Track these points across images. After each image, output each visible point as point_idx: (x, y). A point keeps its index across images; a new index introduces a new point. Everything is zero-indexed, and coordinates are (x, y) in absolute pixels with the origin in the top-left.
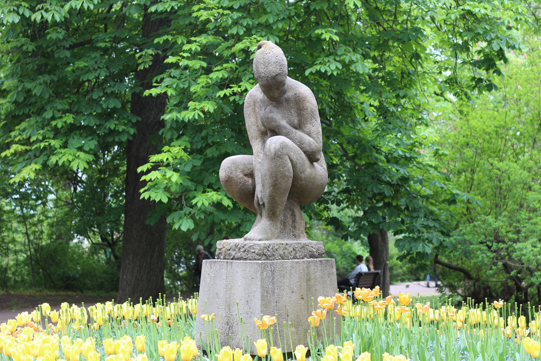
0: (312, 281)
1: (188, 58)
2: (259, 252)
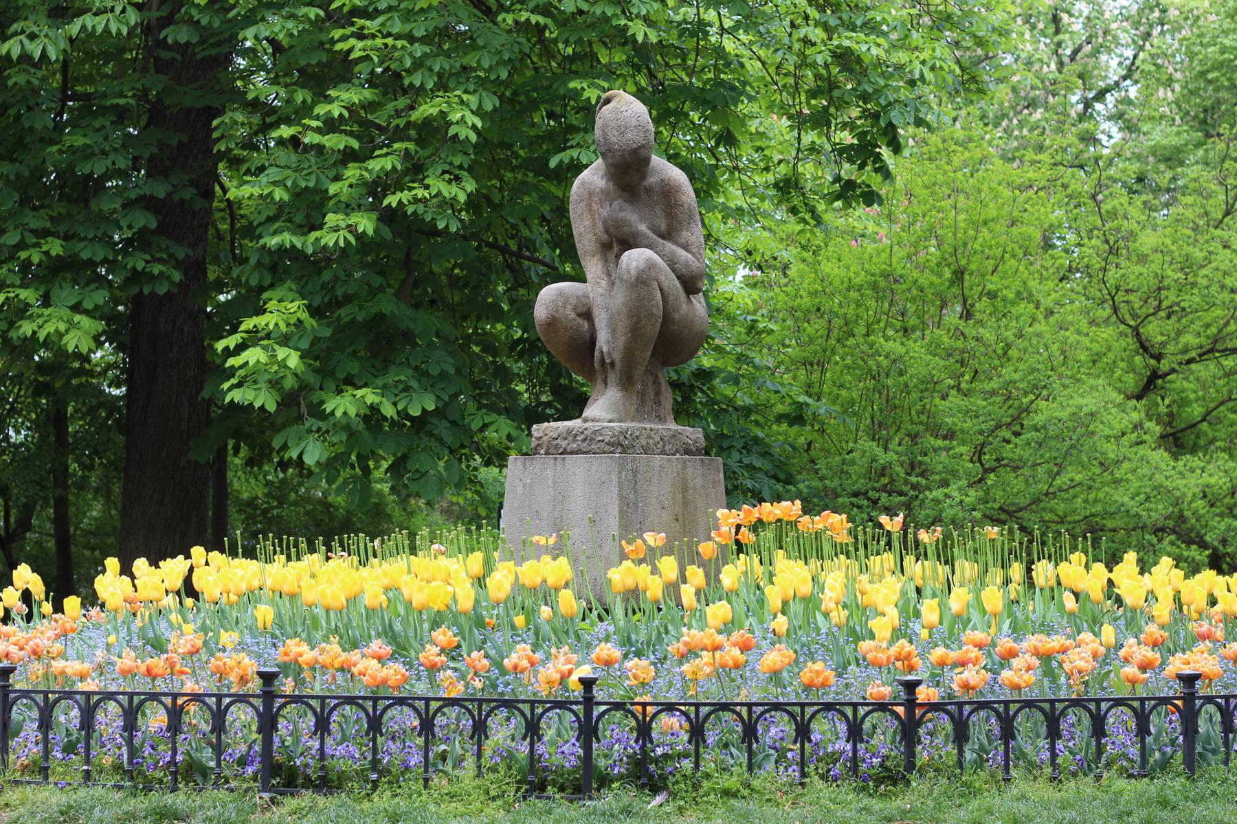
0: (691, 492)
1: (318, 130)
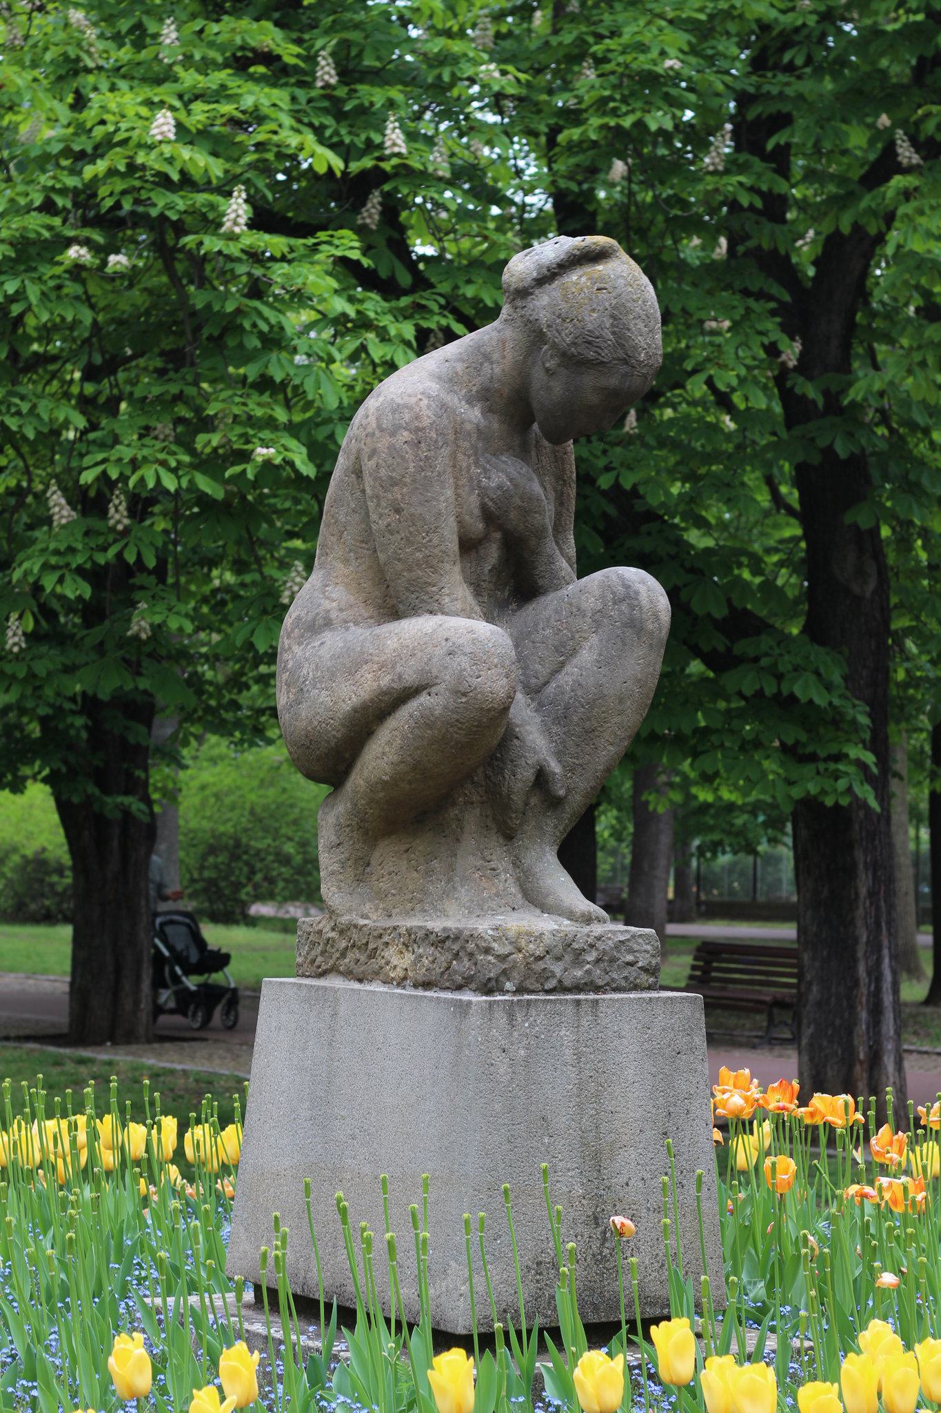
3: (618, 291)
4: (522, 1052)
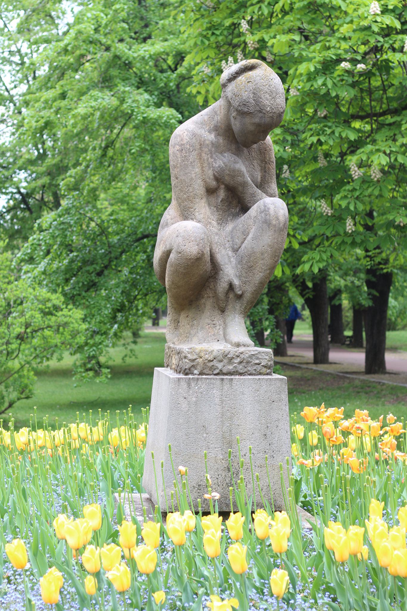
2: (269, 363)
3: (256, 82)
4: (194, 399)
